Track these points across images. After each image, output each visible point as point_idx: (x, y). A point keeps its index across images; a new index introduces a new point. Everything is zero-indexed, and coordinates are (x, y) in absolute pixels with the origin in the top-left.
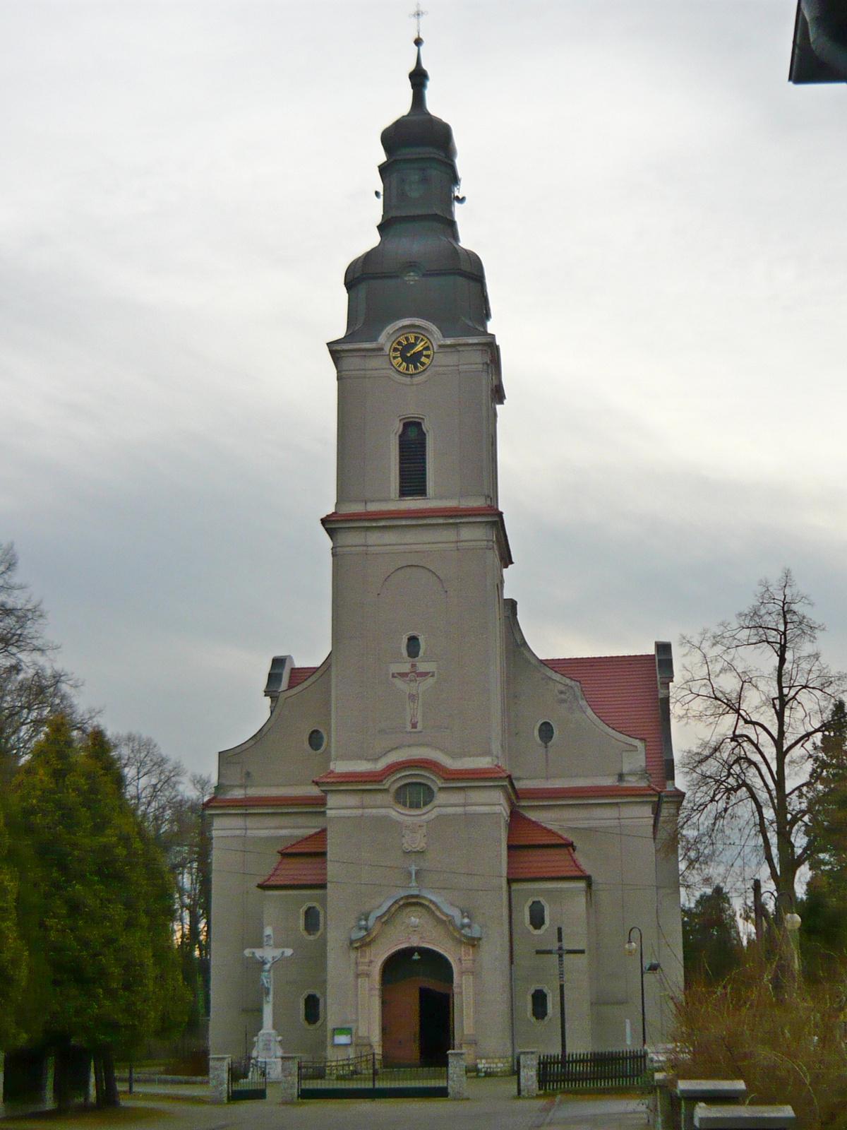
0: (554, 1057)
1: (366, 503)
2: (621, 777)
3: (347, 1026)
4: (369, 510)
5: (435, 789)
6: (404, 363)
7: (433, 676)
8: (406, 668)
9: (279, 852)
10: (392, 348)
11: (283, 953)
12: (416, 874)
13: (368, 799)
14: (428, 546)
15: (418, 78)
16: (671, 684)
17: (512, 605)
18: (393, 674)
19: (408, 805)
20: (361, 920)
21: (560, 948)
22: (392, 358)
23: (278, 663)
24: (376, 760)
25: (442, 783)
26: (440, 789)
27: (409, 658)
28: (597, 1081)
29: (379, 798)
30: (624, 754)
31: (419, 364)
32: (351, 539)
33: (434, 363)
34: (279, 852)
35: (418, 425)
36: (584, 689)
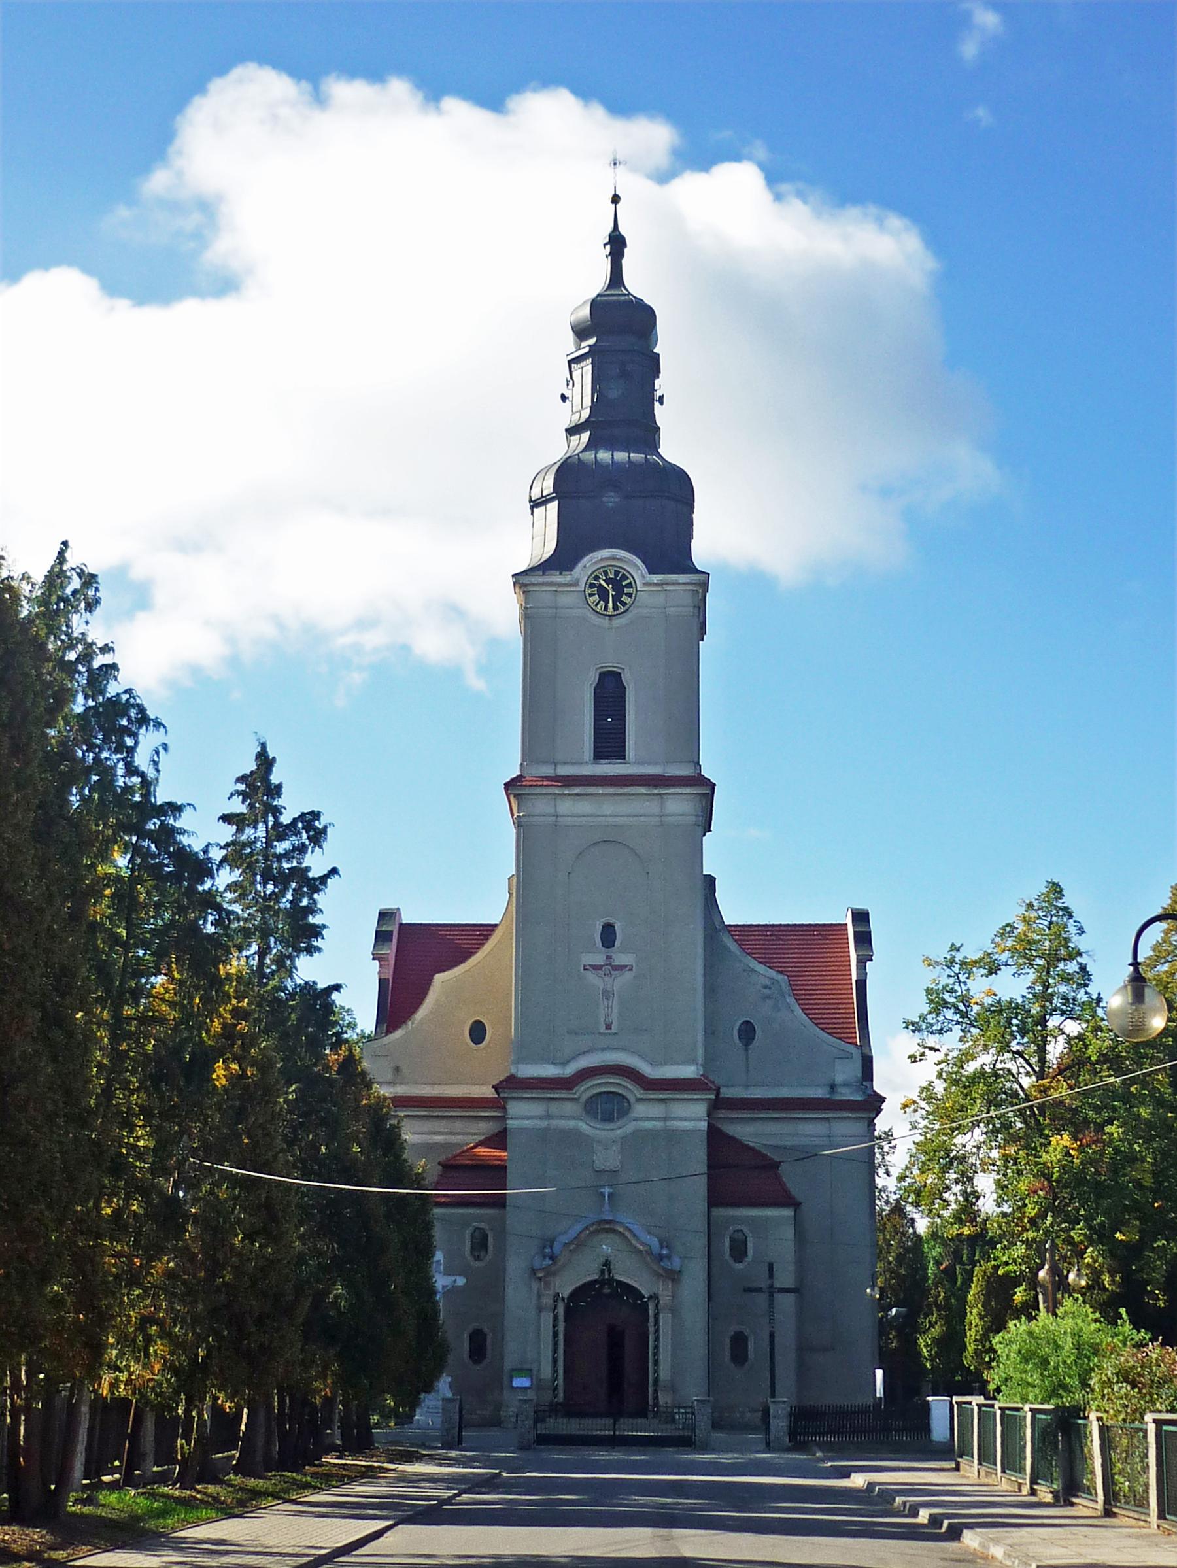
0: (837, 1407)
1: (556, 766)
2: (833, 1087)
3: (527, 1366)
4: (559, 774)
5: (632, 1099)
6: (602, 602)
7: (631, 970)
8: (599, 959)
9: (439, 1163)
10: (588, 583)
11: (455, 1281)
12: (609, 1197)
13: (554, 1108)
14: (625, 819)
15: (617, 244)
16: (868, 963)
17: (710, 881)
18: (585, 966)
19: (599, 1117)
20: (545, 1247)
21: (771, 1286)
22: (587, 595)
23: (385, 916)
24: (564, 1063)
25: (642, 1094)
26: (639, 1100)
27: (603, 949)
28: (869, 1435)
29: (569, 1108)
30: (837, 1060)
31: (619, 604)
32: (541, 806)
33: (636, 603)
34: (439, 1163)
35: (617, 676)
36: (791, 983)
